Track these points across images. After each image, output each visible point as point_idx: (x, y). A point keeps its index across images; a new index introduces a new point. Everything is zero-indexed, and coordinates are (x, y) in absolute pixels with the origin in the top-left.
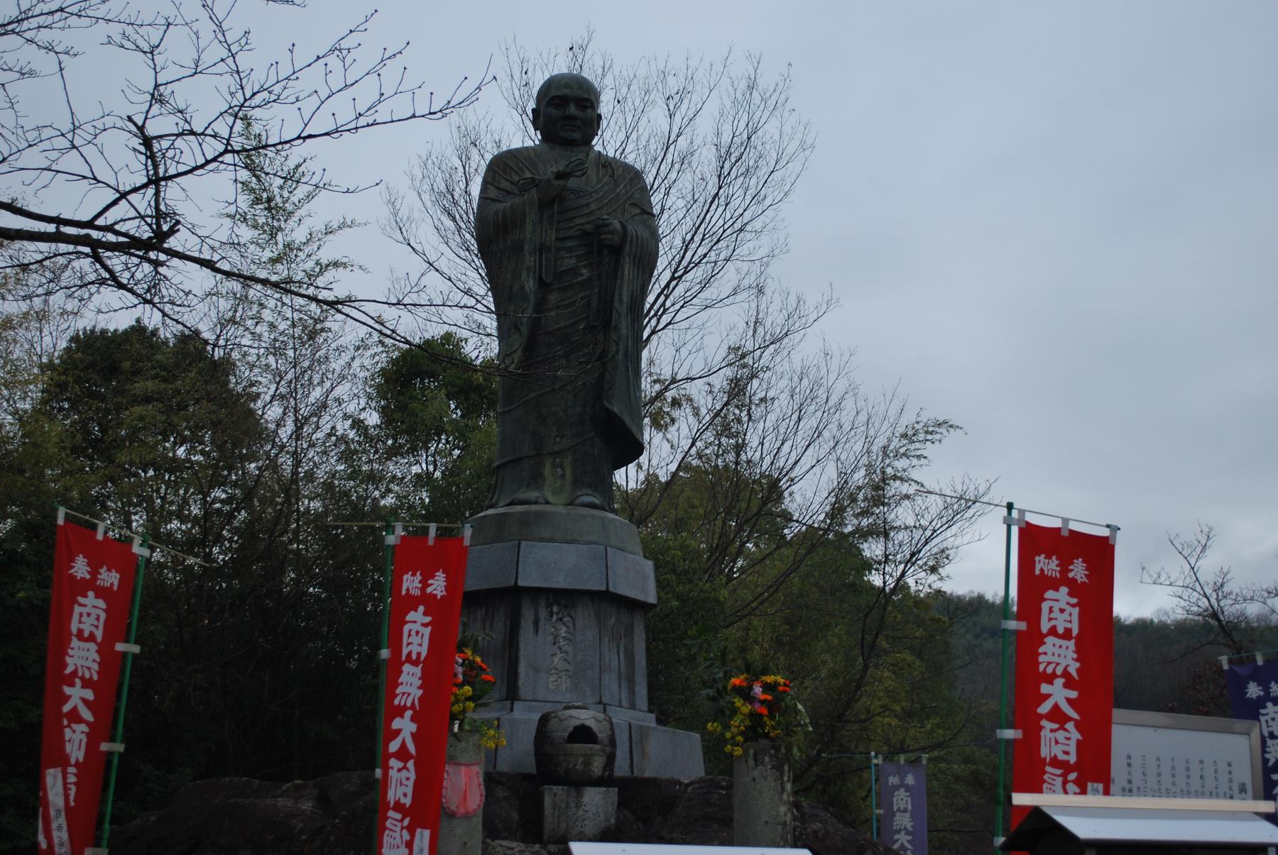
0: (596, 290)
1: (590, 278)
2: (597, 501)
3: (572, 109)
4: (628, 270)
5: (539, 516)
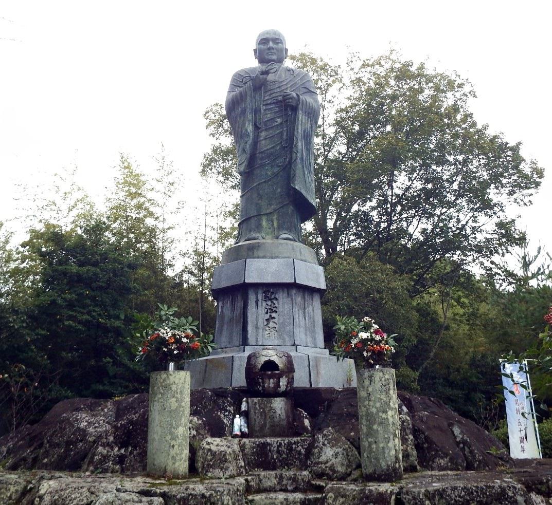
0: (285, 129)
1: (281, 123)
2: (290, 237)
3: (271, 44)
4: (301, 116)
5: (258, 246)
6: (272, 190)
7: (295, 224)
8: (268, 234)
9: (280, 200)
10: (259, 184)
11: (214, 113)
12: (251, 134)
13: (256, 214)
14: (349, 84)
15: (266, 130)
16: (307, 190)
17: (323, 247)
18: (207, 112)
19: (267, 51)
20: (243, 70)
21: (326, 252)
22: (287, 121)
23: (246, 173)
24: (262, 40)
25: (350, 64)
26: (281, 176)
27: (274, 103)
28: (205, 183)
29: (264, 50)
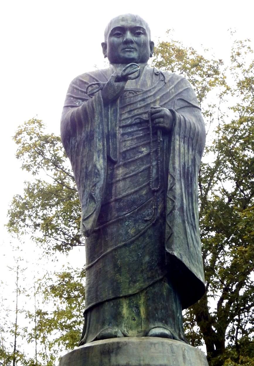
0: (154, 163)
1: (148, 154)
2: (167, 332)
3: (129, 36)
4: (179, 144)
6: (136, 258)
7: (173, 312)
8: (131, 328)
9: (150, 273)
10: (115, 250)
11: (29, 134)
12: (102, 172)
13: (111, 296)
14: (236, 88)
15: (125, 165)
16: (191, 256)
17: (203, 341)
18: (19, 133)
19: (122, 46)
20: (87, 75)
21: (208, 350)
22: (156, 152)
23: (95, 231)
24: (115, 29)
25: (237, 57)
26: (150, 237)
27: (136, 124)
28: (16, 242)
29: (119, 44)
